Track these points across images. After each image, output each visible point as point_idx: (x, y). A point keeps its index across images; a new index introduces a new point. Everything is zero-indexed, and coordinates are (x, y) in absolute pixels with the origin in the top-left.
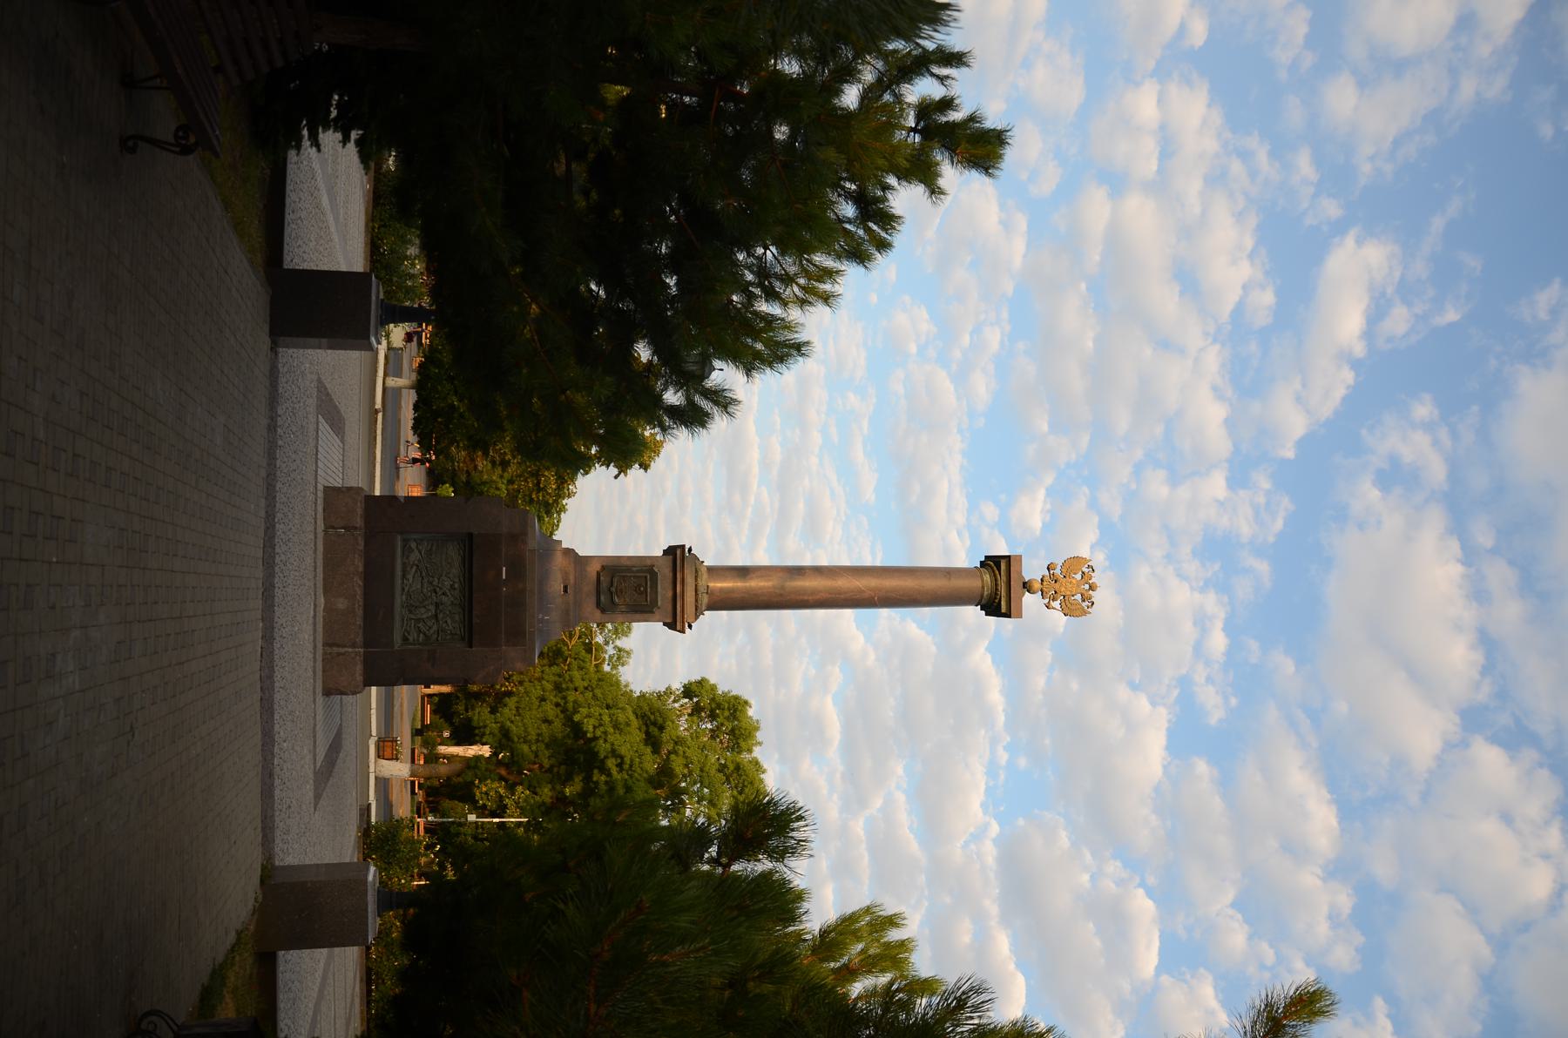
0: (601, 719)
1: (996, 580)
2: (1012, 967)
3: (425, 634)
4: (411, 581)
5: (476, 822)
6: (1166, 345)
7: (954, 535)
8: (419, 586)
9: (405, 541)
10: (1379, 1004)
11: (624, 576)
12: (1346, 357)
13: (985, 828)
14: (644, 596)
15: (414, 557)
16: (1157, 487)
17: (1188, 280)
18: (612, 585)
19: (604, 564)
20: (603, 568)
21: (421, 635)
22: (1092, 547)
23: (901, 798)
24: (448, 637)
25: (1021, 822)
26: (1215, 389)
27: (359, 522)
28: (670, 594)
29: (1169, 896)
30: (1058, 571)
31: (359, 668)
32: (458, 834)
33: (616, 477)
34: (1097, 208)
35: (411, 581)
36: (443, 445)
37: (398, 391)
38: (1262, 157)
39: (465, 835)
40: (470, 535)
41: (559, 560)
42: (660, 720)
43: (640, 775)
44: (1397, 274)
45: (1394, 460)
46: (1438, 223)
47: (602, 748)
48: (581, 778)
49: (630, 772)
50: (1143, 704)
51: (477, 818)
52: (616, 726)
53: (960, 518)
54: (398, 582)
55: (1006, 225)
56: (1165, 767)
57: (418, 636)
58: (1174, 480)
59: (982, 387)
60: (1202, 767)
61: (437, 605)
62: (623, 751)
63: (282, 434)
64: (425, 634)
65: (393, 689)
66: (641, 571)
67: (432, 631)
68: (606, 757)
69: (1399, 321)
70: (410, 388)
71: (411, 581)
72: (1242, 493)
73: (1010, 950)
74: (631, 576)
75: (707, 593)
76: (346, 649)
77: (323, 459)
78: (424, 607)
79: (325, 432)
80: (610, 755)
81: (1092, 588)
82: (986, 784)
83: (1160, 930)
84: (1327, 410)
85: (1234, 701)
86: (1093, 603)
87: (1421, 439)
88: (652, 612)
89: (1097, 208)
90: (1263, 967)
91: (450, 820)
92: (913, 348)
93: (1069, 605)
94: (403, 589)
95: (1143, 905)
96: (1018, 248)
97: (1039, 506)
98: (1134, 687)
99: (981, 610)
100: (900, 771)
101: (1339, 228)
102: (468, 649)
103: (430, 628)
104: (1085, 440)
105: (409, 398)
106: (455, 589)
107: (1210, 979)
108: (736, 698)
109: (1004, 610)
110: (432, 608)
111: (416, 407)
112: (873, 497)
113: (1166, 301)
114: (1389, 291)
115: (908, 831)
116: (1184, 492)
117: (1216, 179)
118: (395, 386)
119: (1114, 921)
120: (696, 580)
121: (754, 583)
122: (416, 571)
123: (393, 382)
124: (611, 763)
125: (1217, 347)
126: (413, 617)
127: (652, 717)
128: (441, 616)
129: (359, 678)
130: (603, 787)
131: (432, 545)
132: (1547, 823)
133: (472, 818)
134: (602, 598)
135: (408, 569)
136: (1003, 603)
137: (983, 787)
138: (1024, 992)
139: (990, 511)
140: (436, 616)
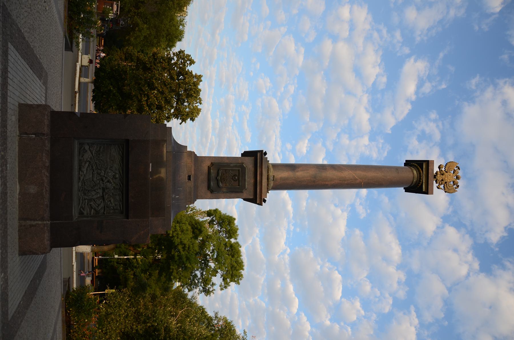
0: (176, 229)
1: (420, 174)
2: (294, 295)
3: (95, 209)
4: (85, 173)
5: (118, 258)
6: (349, 93)
7: (277, 154)
8: (91, 176)
9: (81, 145)
10: (412, 309)
11: (226, 170)
12: (408, 100)
13: (285, 251)
14: (238, 182)
15: (88, 156)
16: (345, 140)
17: (358, 72)
18: (218, 175)
19: (213, 162)
20: (212, 164)
21: (93, 210)
22: (323, 160)
23: (258, 240)
24: (111, 211)
25: (297, 248)
26: (366, 109)
27: (46, 130)
28: (252, 181)
29: (346, 274)
30: (443, 169)
32: (111, 262)
33: (181, 124)
34: (328, 46)
35: (85, 173)
36: (106, 108)
37: (86, 84)
38: (384, 31)
39: (114, 262)
40: (127, 141)
41: (186, 160)
42: (199, 227)
43: (193, 252)
44: (427, 73)
45: (423, 132)
46: (441, 55)
47: (177, 241)
48: (166, 252)
49: (188, 251)
50: (339, 212)
51: (118, 256)
52: (182, 231)
53: (279, 149)
54: (76, 173)
55: (297, 51)
56: (346, 232)
57: (90, 211)
58: (351, 139)
59: (287, 105)
60: (357, 232)
61: (104, 189)
62: (185, 242)
64: (95, 209)
65: (73, 248)
66: (236, 166)
67: (100, 208)
68: (178, 244)
69: (427, 88)
70: (91, 83)
71: (85, 172)
72: (373, 143)
73: (293, 290)
74: (230, 170)
75: (273, 180)
76: (36, 222)
78: (95, 191)
79: (14, 57)
80: (180, 244)
81: (458, 178)
82: (286, 236)
83: (342, 285)
84: (401, 117)
85: (369, 211)
87: (432, 125)
88: (242, 192)
89: (328, 46)
90: (376, 297)
91: (108, 257)
92: (265, 92)
93: (448, 187)
94: (79, 178)
95: (337, 276)
96: (301, 59)
97: (306, 145)
98: (336, 206)
100: (257, 231)
101: (409, 56)
102: (125, 220)
103: (99, 205)
104: (321, 125)
105: (91, 87)
106: (116, 178)
107: (358, 300)
108: (231, 217)
109: (424, 190)
110: (100, 191)
111: (94, 91)
112: (250, 141)
113: (350, 78)
114: (425, 78)
115: (260, 251)
116: (354, 143)
117: (368, 38)
118: (84, 81)
119: (328, 281)
120: (268, 172)
121: (299, 174)
122: (89, 165)
123: (83, 80)
124: (180, 247)
126: (86, 197)
127: (196, 226)
128: (106, 197)
129: (47, 242)
130: (177, 258)
131: (100, 147)
132: (468, 252)
133: (116, 256)
134: (212, 184)
135: (83, 164)
136: (424, 186)
137: (285, 237)
138: (298, 304)
139: (289, 146)
140: (103, 197)
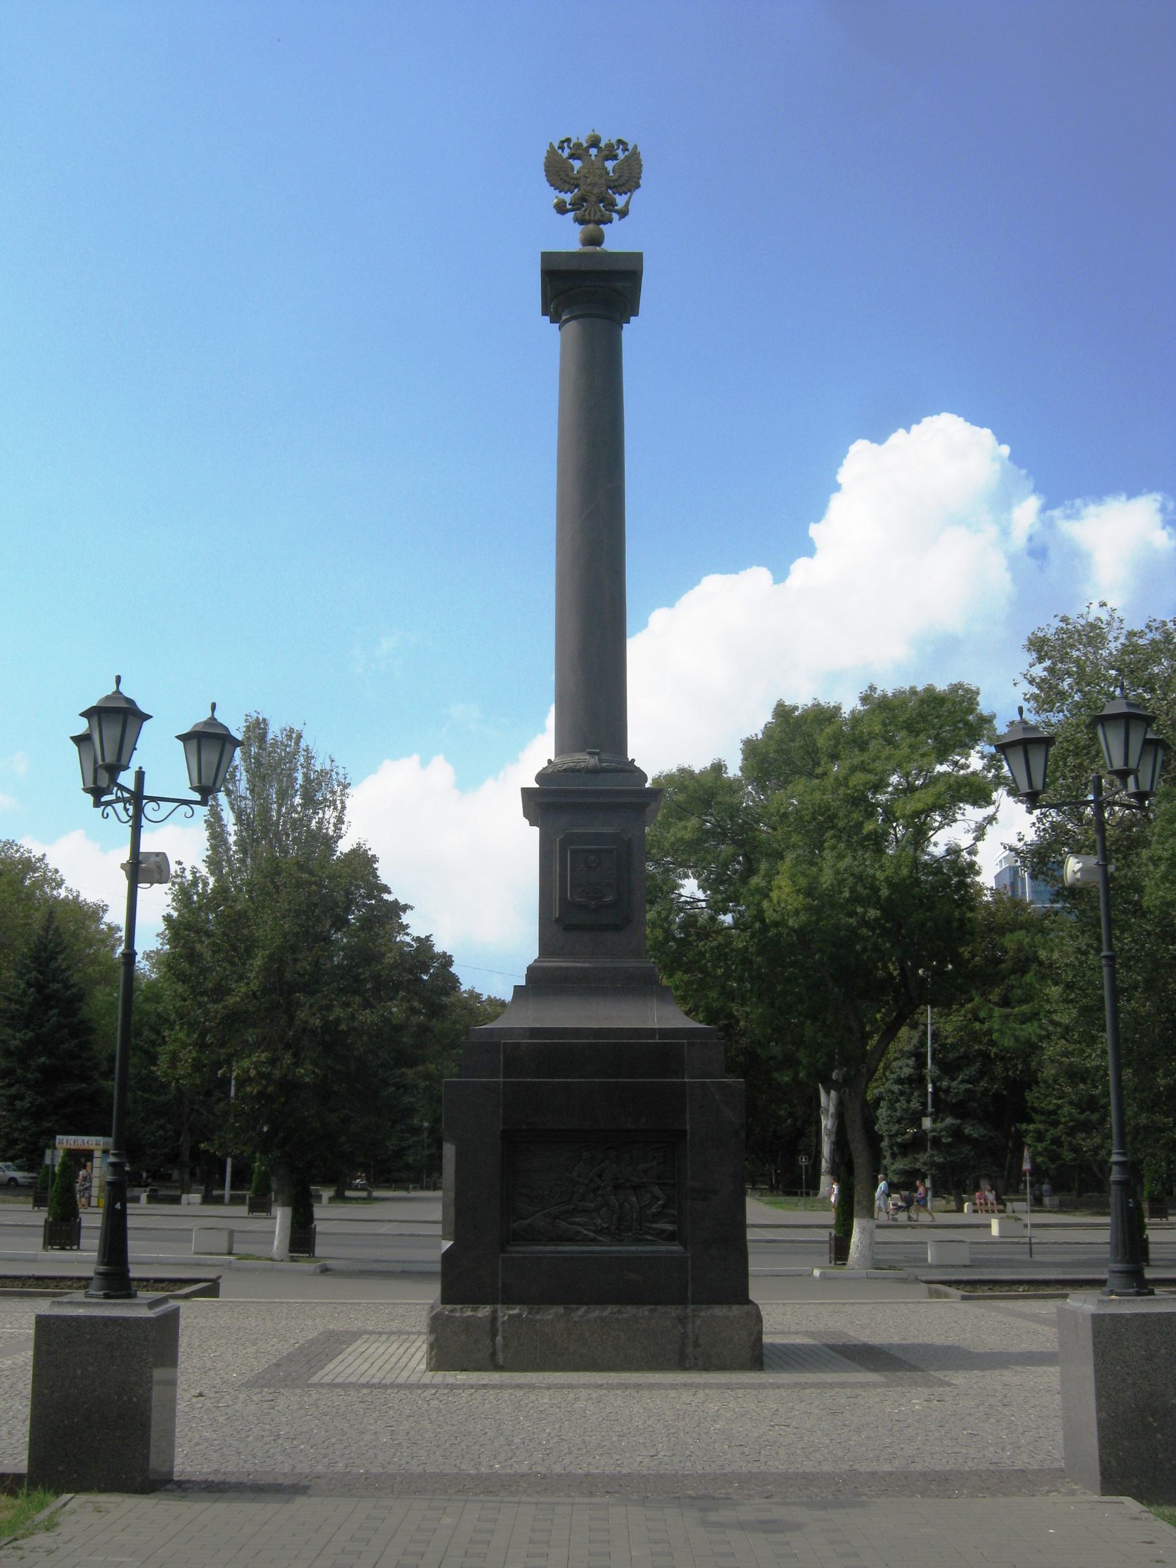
30: (568, 197)
31: (719, 1311)
63: (326, 1461)
64: (664, 1206)
77: (380, 1375)
81: (595, 142)
86: (620, 142)
99: (628, 322)
125: (1019, 898)
129: (736, 1310)
